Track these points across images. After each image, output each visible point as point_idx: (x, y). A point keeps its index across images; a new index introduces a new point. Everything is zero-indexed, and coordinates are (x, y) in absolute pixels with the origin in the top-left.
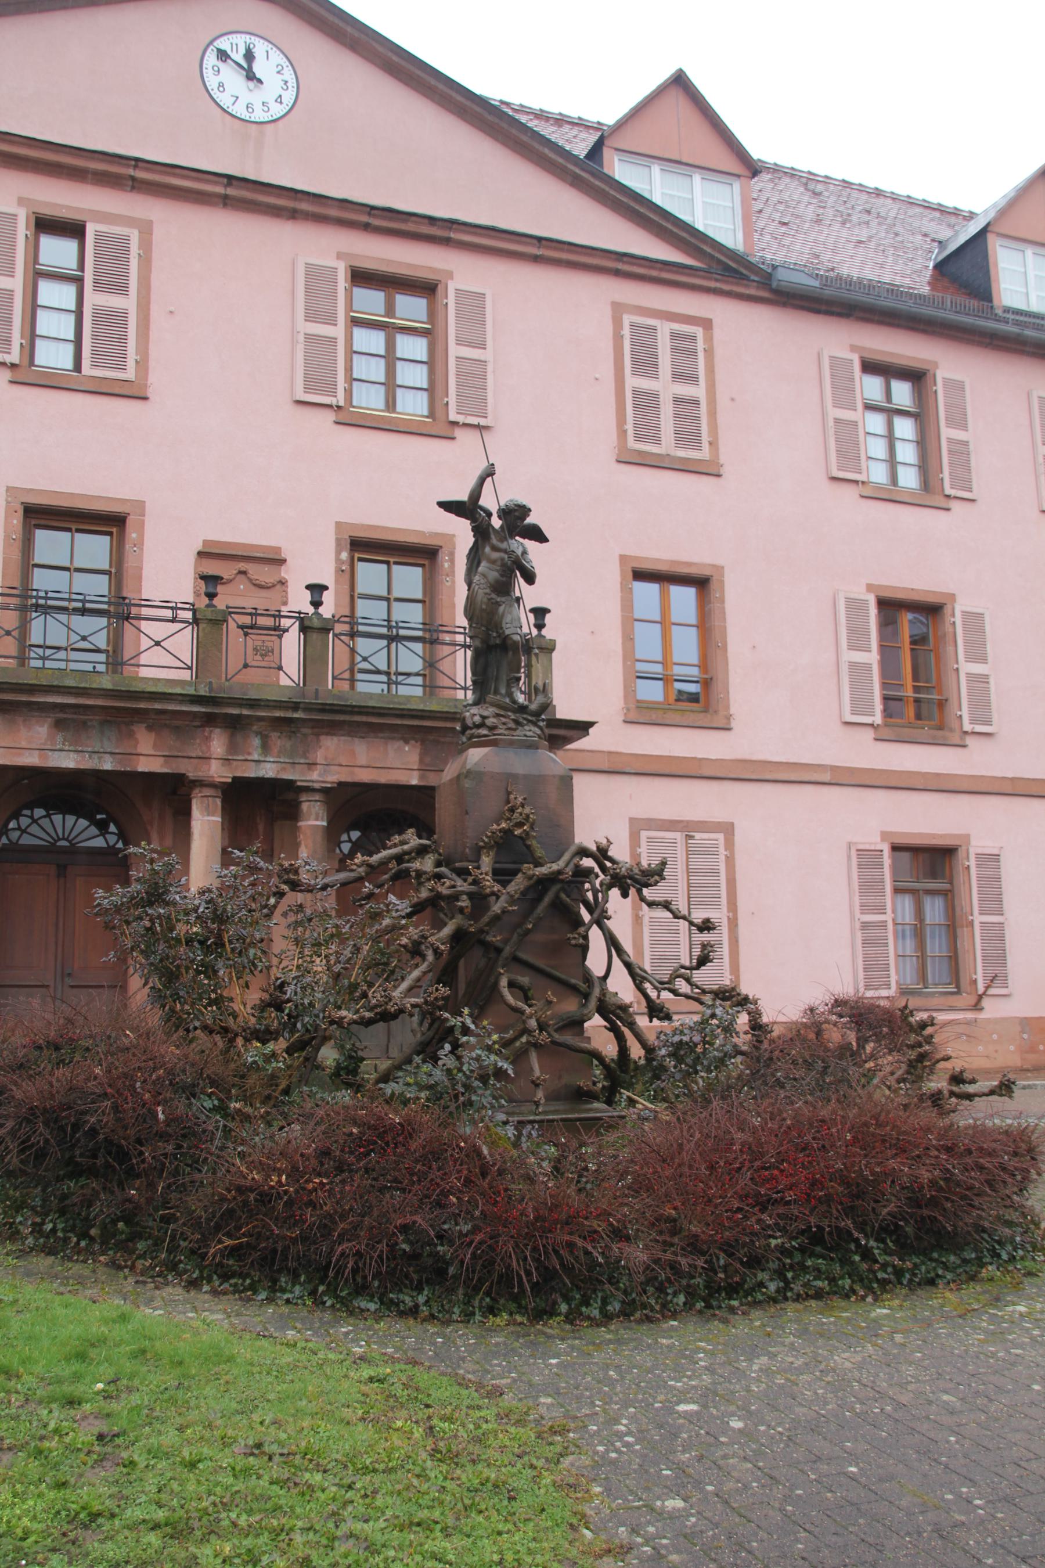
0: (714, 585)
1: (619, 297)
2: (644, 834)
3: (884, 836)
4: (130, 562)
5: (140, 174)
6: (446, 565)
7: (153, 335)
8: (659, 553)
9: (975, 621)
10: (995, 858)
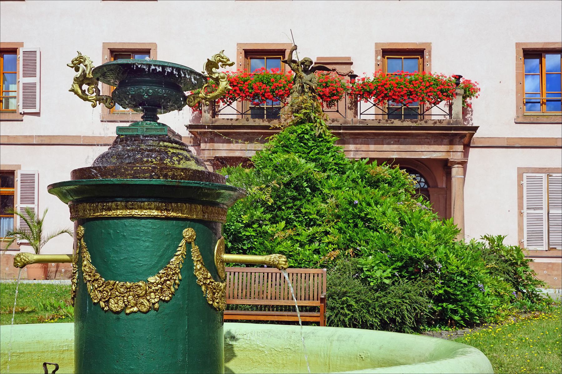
2: (525, 175)
6: (427, 57)
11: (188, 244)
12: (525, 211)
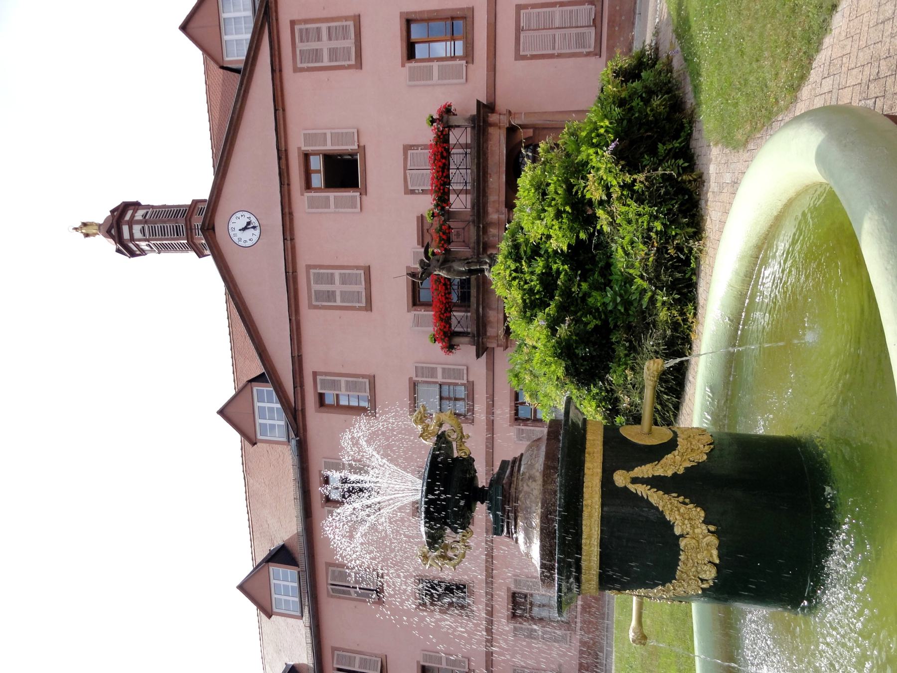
0: (410, 18)
4: (426, 16)
5: (291, 271)
7: (346, 264)
8: (398, 48)
11: (635, 481)
12: (556, 52)
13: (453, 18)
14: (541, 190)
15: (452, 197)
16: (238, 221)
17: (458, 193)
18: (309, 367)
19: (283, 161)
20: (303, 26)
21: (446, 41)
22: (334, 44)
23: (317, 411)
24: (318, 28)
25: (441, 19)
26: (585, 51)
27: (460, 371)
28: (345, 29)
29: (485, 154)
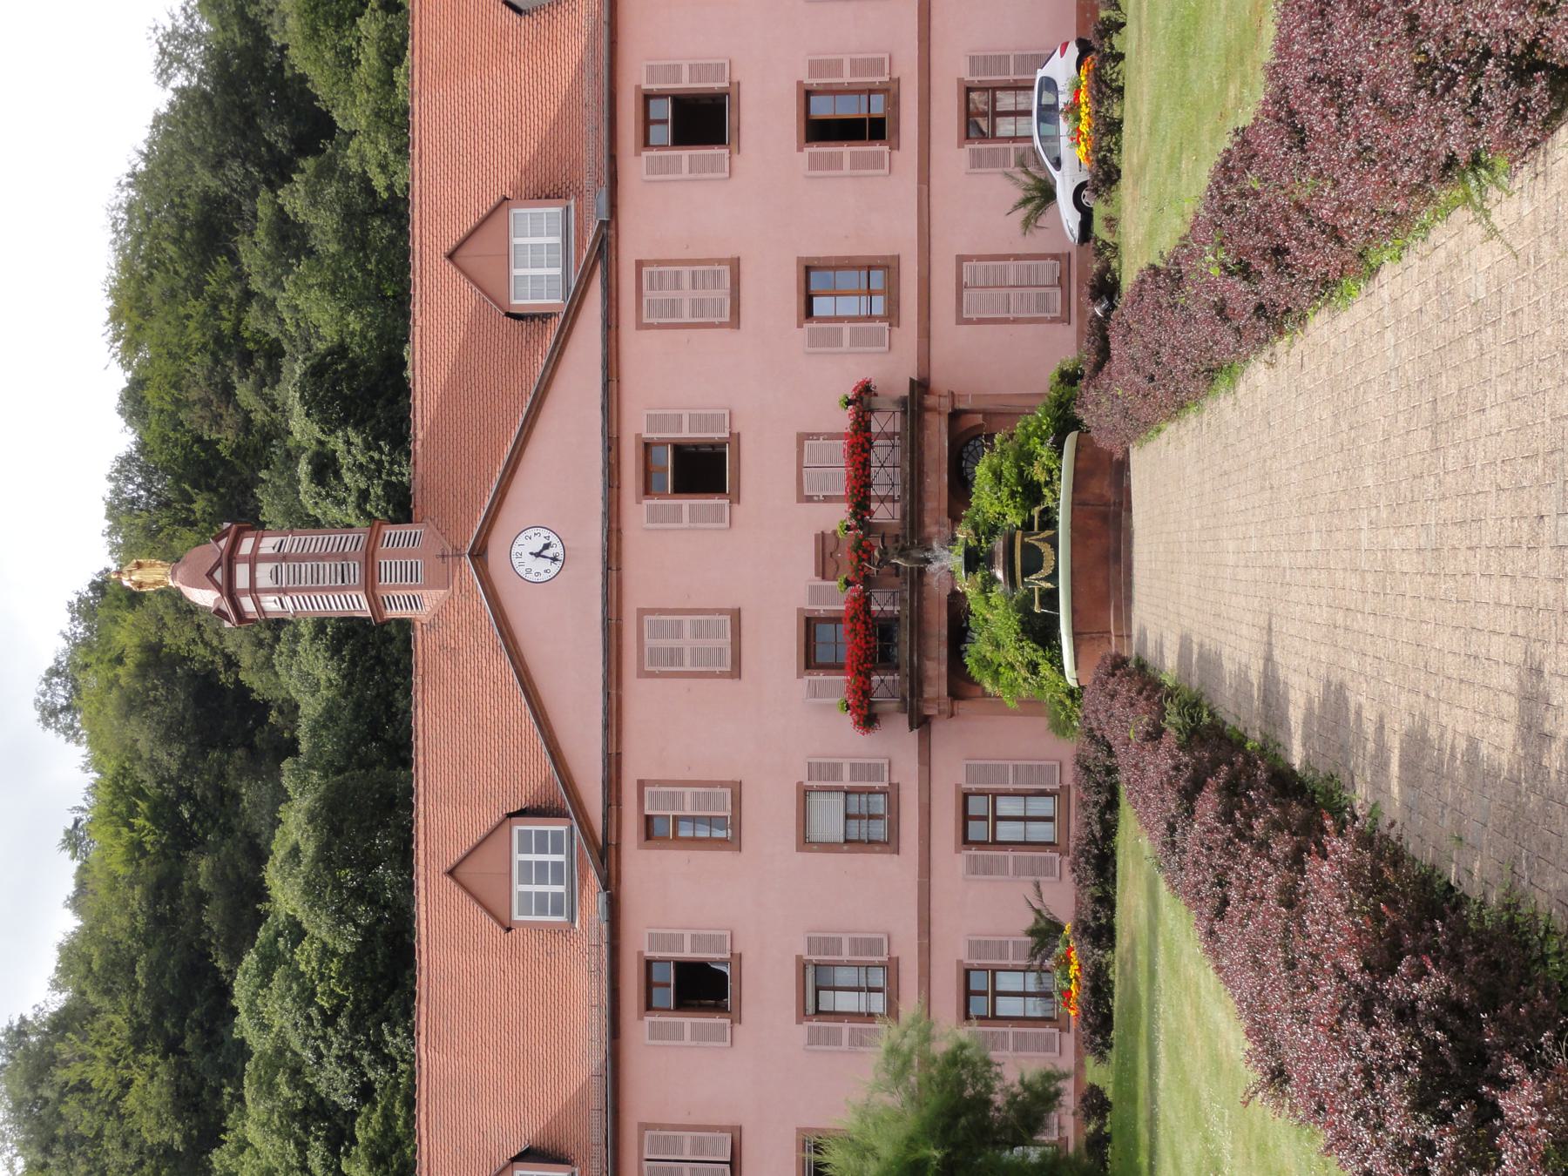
1: (633, 325)
3: (960, 146)
8: (793, 303)
9: (815, 67)
10: (972, 59)
12: (1011, 316)
13: (870, 268)
14: (998, 476)
15: (873, 506)
16: (529, 543)
17: (882, 500)
18: (632, 773)
19: (614, 452)
20: (655, 269)
21: (860, 295)
22: (700, 294)
23: (640, 847)
24: (677, 273)
25: (853, 268)
26: (1048, 316)
27: (878, 767)
28: (717, 275)
29: (920, 447)
